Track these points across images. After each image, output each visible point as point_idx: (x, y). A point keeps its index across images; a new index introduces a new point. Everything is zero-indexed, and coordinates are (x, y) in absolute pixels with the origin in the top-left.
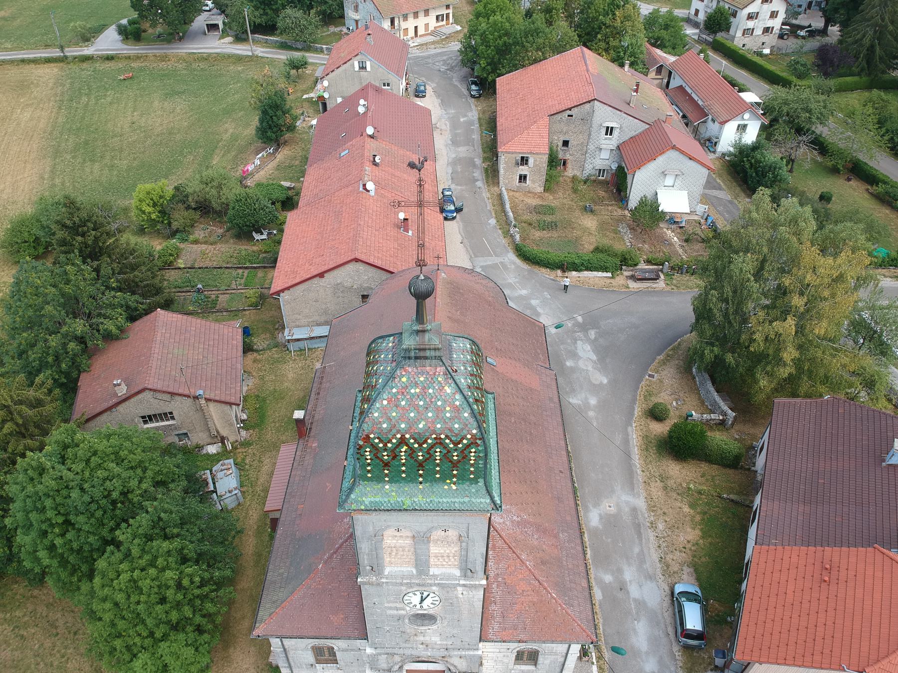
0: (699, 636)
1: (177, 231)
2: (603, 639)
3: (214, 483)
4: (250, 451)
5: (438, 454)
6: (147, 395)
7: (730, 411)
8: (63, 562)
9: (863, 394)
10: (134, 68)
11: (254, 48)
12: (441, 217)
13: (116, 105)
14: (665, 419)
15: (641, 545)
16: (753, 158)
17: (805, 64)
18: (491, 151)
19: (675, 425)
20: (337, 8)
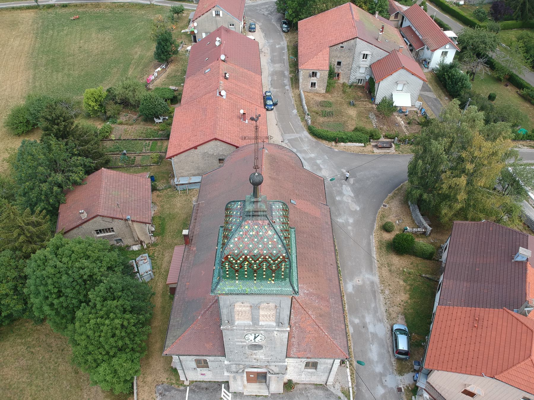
0: (405, 353)
1: (110, 117)
2: (353, 354)
3: (137, 268)
4: (157, 248)
5: (265, 266)
6: (98, 218)
7: (429, 227)
8: (58, 313)
9: (505, 217)
12: (265, 110)
13: (69, 36)
14: (391, 231)
15: (376, 302)
16: (450, 73)
17: (484, 13)
18: (295, 66)
19: (397, 235)
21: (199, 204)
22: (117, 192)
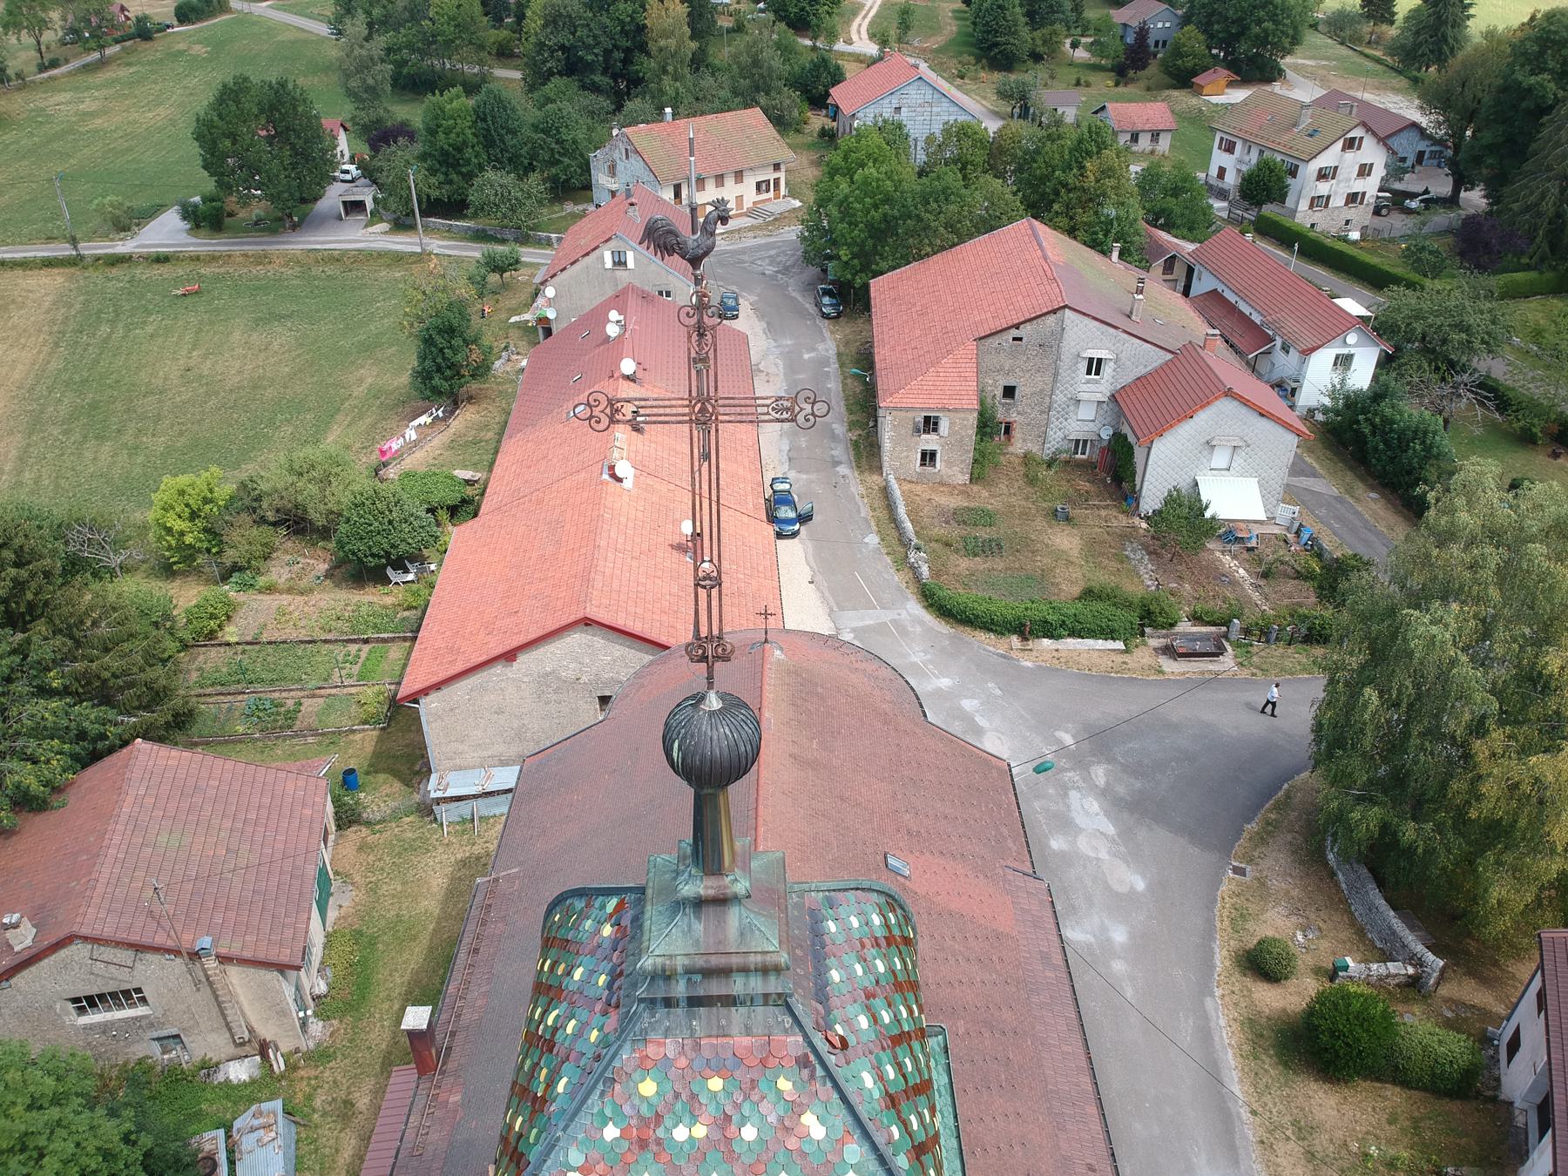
1: (236, 568)
4: (327, 1073)
6: (78, 951)
10: (204, 275)
11: (426, 240)
12: (770, 530)
13: (160, 340)
14: (1286, 978)
20: (579, 171)
21: (496, 880)
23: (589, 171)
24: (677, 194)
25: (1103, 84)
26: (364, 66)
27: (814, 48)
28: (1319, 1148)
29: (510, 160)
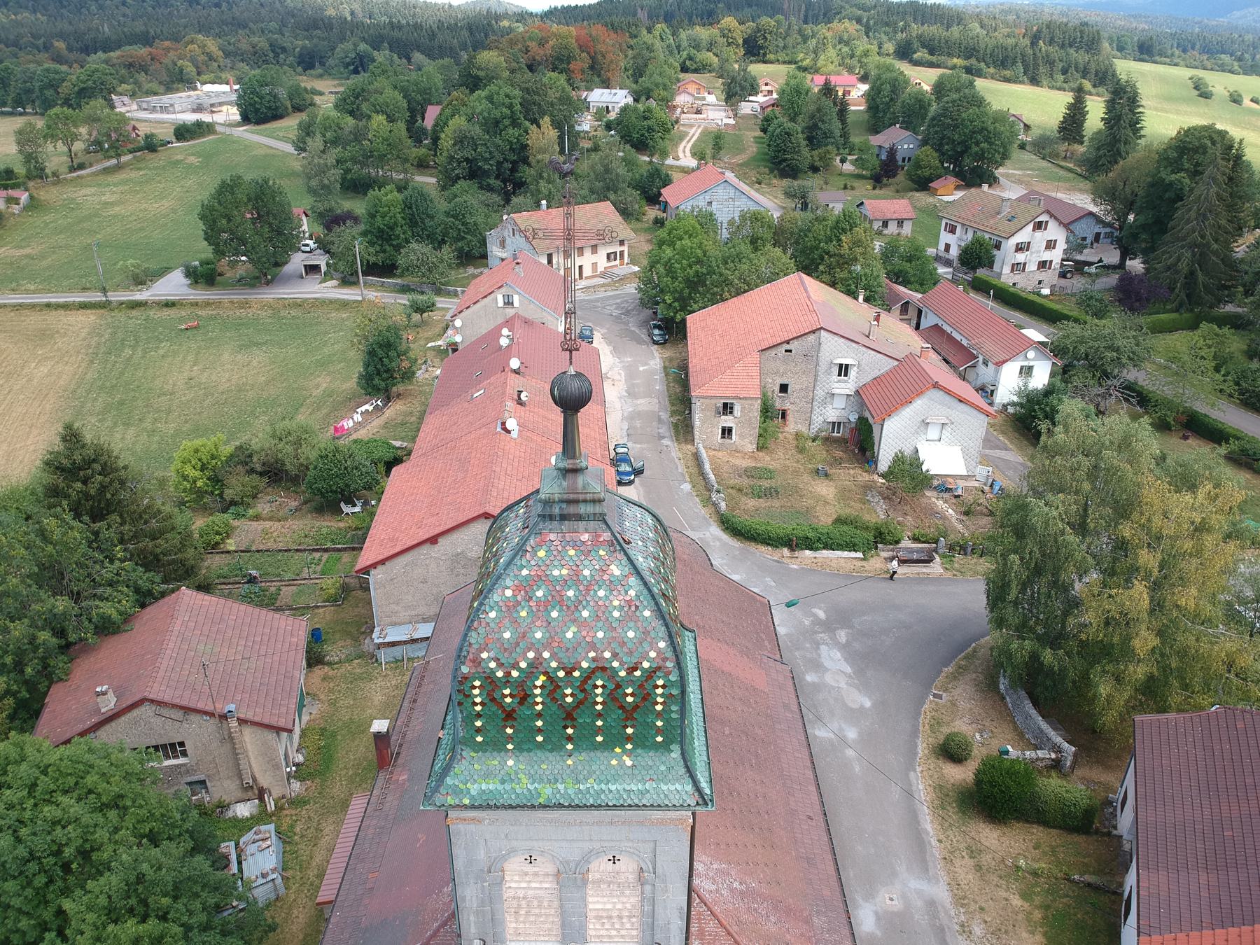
1: (233, 503)
3: (240, 863)
4: (304, 812)
5: (599, 691)
6: (146, 711)
7: (1066, 745)
11: (365, 292)
13: (170, 359)
14: (966, 759)
20: (478, 245)
22: (209, 646)
23: (485, 245)
24: (550, 262)
25: (864, 187)
26: (322, 171)
27: (651, 162)
28: (985, 863)
29: (428, 236)
